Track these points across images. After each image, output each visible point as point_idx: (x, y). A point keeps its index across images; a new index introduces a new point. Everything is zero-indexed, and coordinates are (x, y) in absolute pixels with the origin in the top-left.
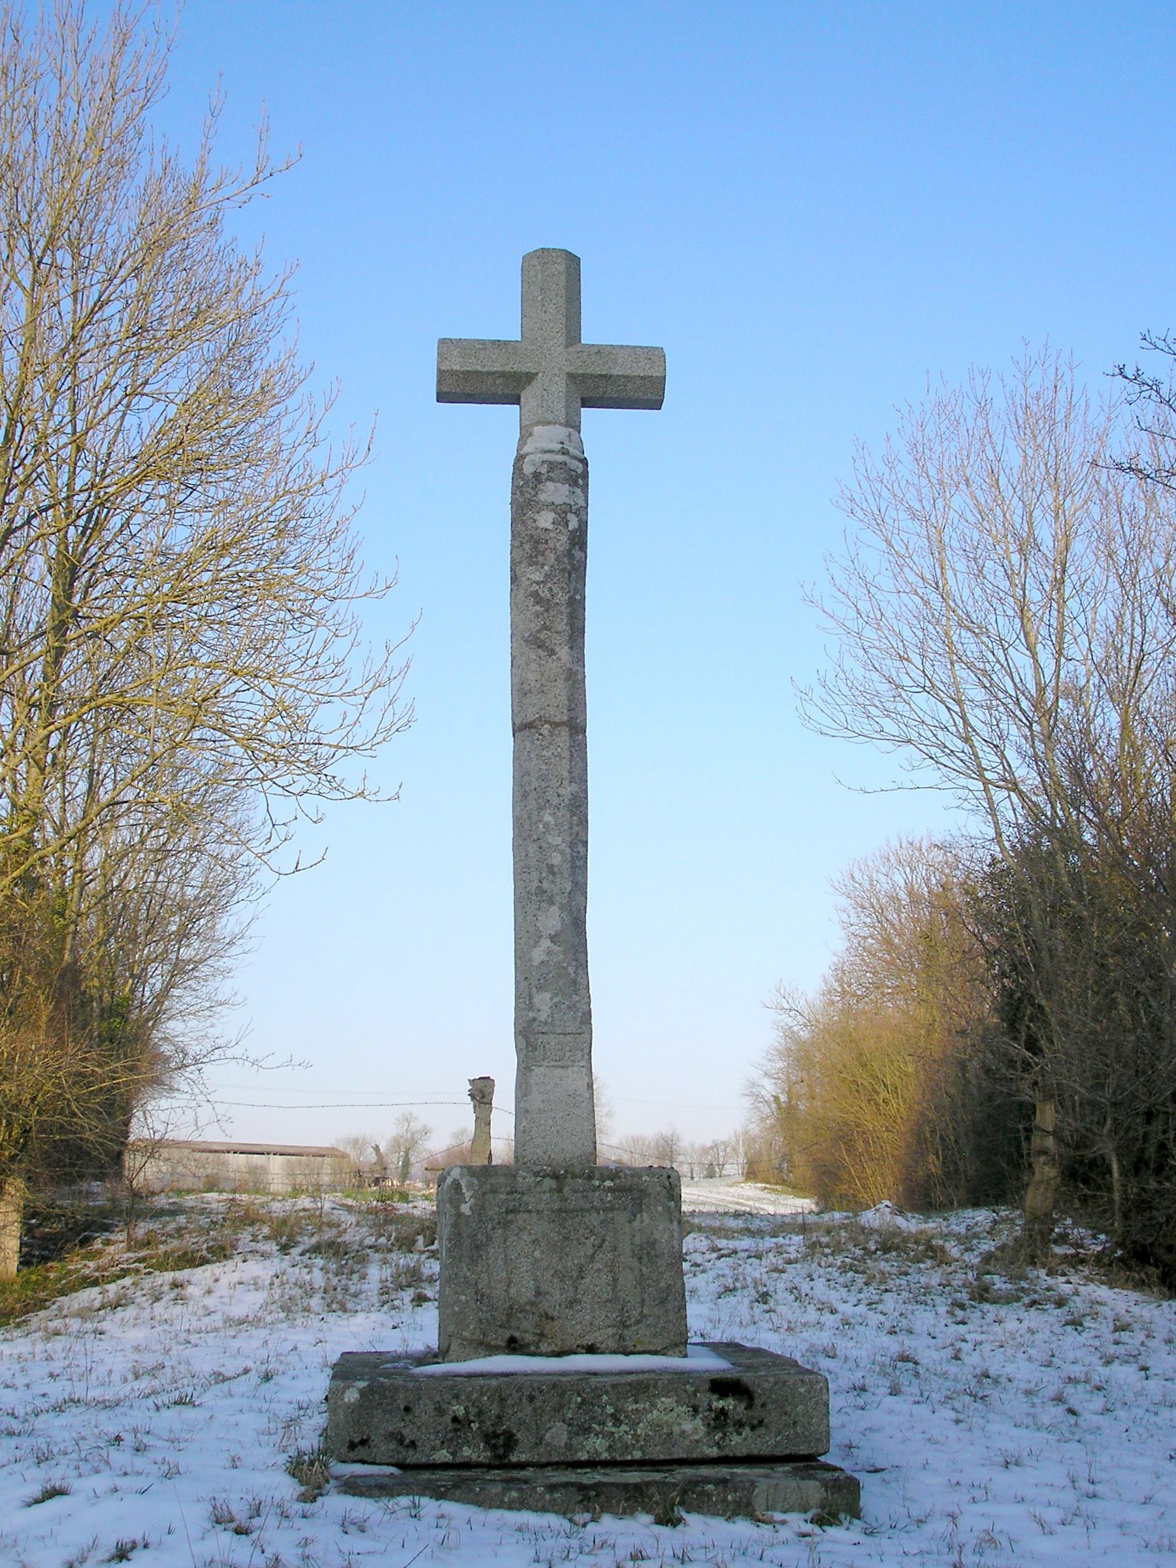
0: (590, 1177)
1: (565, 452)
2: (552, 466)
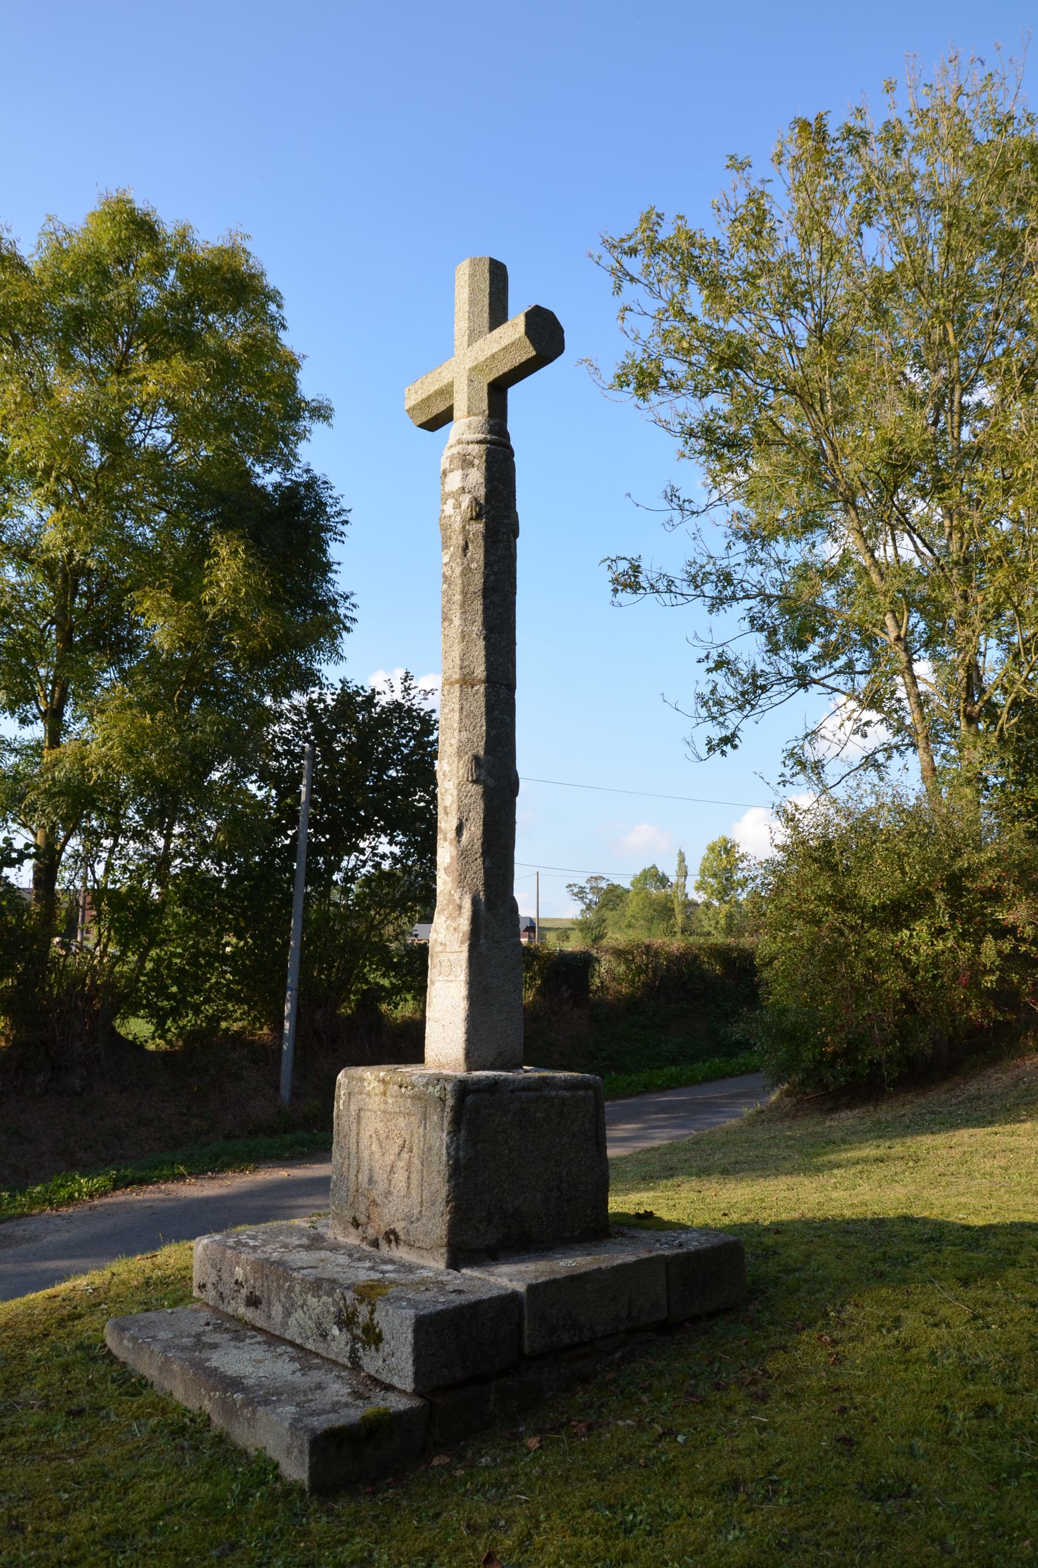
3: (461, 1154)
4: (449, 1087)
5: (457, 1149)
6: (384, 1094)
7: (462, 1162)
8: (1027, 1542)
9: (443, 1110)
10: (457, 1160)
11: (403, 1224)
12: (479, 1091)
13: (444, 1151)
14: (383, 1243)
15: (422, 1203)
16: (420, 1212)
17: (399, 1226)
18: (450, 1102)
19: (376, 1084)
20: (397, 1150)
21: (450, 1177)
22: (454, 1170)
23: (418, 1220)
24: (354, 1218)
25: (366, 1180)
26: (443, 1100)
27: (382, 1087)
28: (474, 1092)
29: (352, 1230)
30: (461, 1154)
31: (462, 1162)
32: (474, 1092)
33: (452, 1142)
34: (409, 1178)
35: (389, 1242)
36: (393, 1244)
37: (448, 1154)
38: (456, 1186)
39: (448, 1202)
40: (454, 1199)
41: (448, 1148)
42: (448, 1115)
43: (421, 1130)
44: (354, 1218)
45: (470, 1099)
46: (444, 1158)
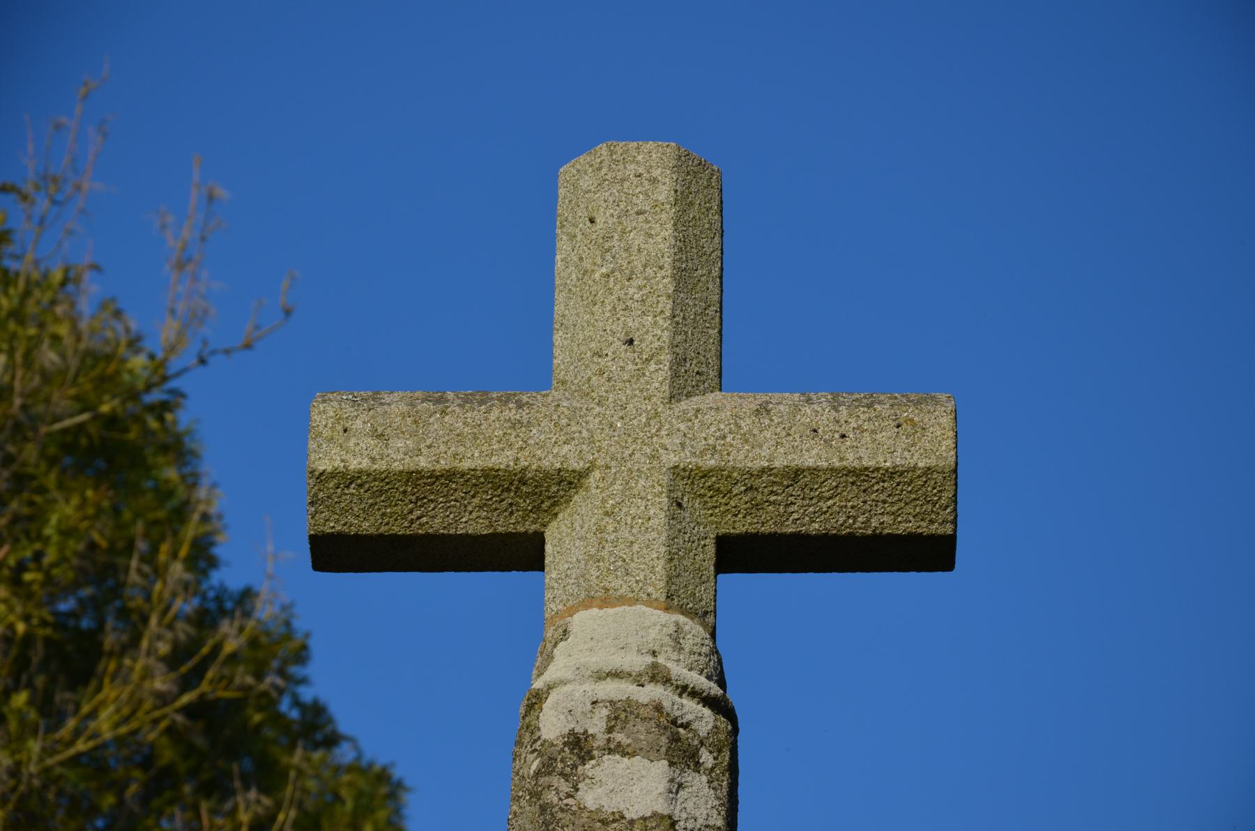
1: (657, 675)
2: (621, 713)
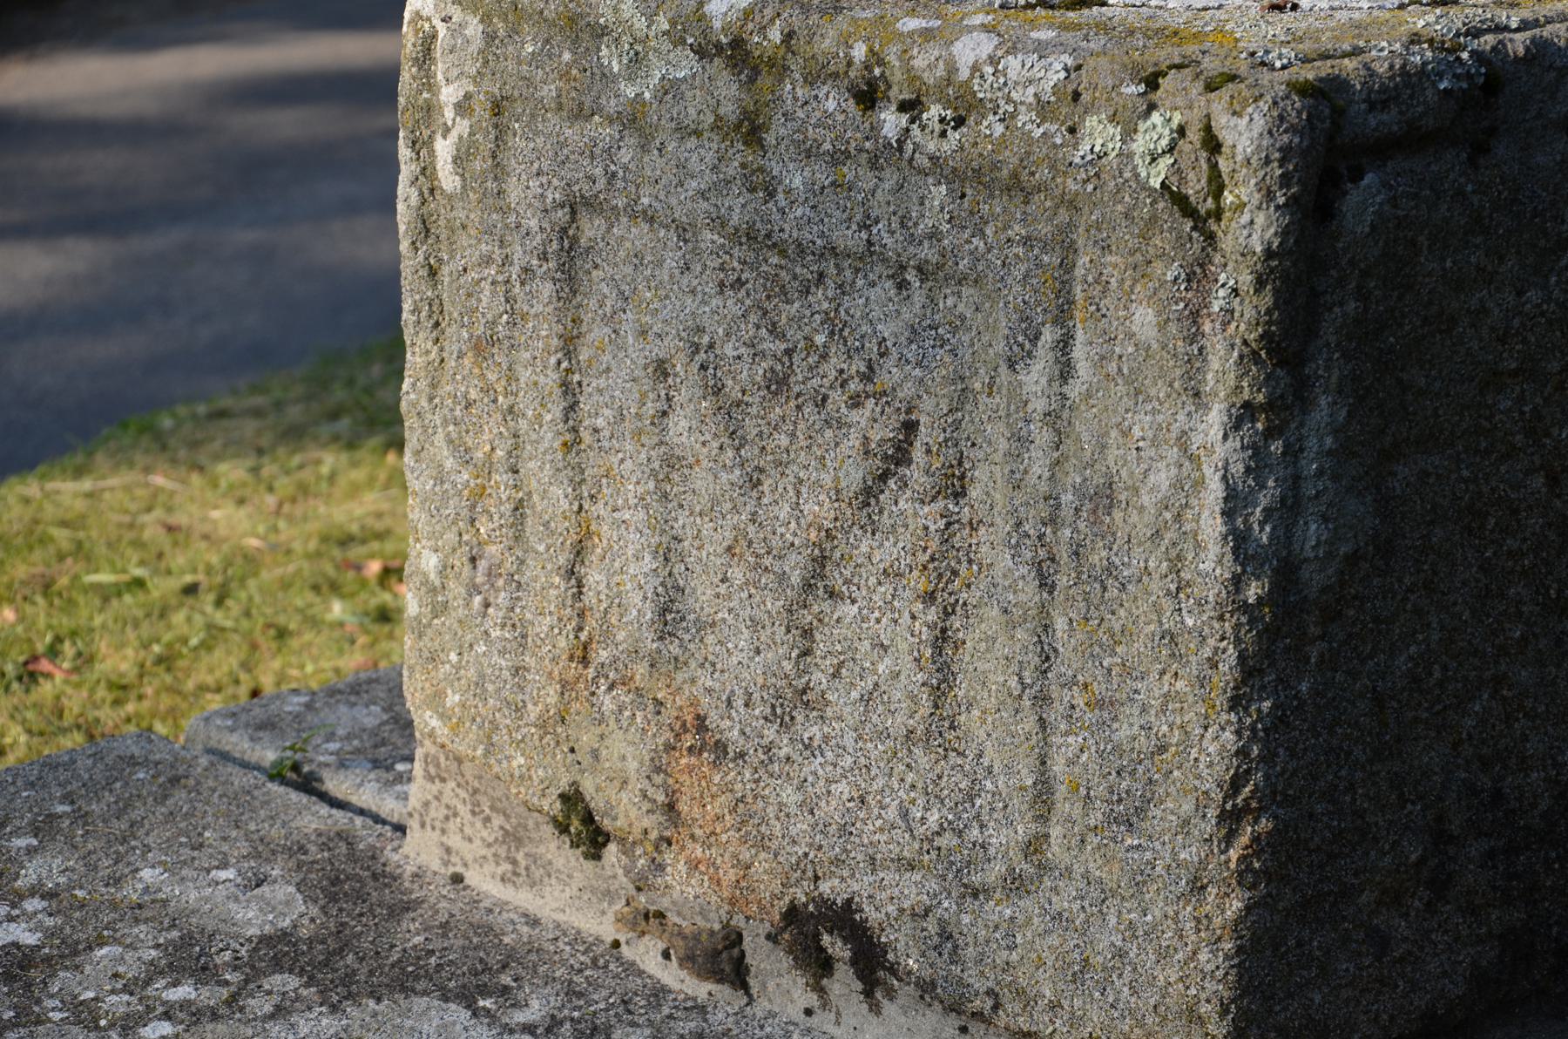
0: (868, 97)
3: (1312, 532)
4: (1244, 134)
5: (1287, 511)
6: (751, 130)
7: (1314, 579)
8: (1413, 857)
9: (1198, 275)
10: (1286, 573)
11: (912, 889)
12: (1412, 140)
13: (1211, 526)
14: (770, 965)
15: (1043, 797)
16: (1034, 846)
17: (886, 898)
18: (1251, 226)
19: (685, 65)
20: (854, 476)
21: (1249, 670)
22: (1270, 635)
23: (1016, 885)
24: (572, 799)
25: (639, 606)
26: (1198, 216)
27: (728, 91)
28: (1381, 149)
29: (561, 855)
30: (1312, 532)
31: (1314, 579)
32: (1381, 149)
33: (1258, 465)
34: (942, 637)
35: (819, 966)
36: (843, 983)
37: (1239, 541)
38: (1278, 722)
39: (1231, 819)
40: (1269, 799)
41: (1234, 504)
42: (1236, 301)
43: (1036, 377)
44: (572, 799)
45: (1363, 201)
46: (1211, 559)
